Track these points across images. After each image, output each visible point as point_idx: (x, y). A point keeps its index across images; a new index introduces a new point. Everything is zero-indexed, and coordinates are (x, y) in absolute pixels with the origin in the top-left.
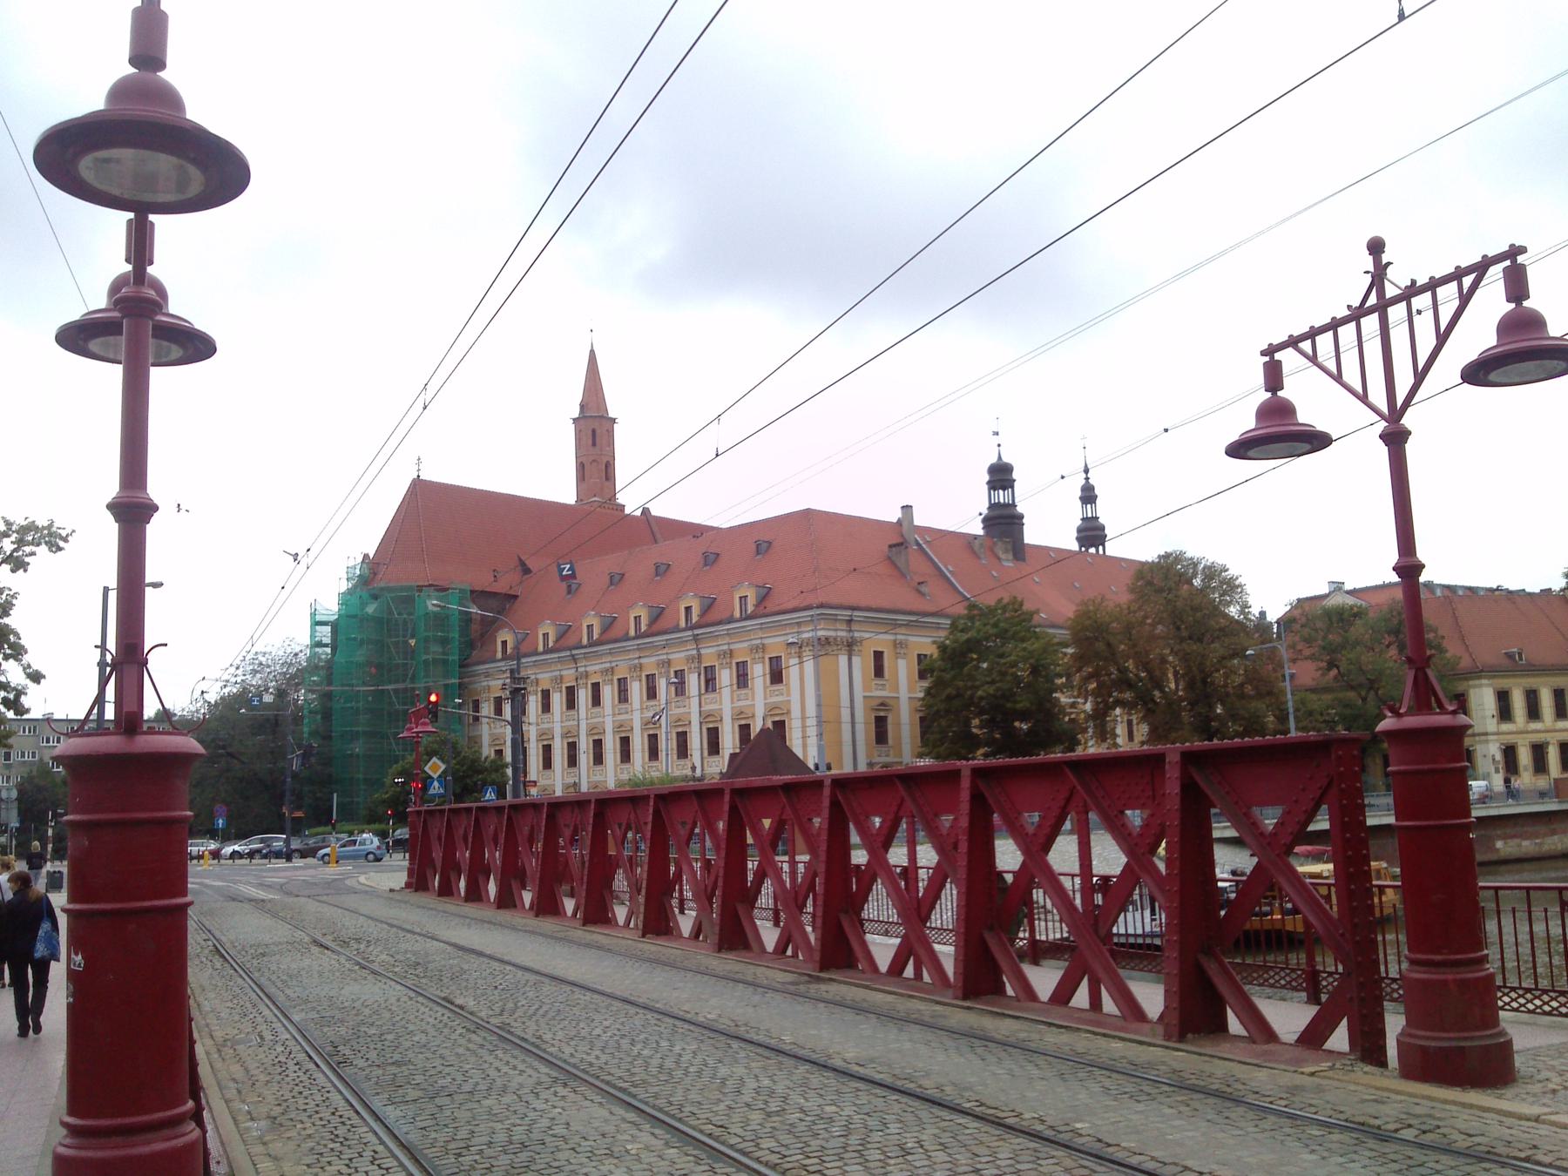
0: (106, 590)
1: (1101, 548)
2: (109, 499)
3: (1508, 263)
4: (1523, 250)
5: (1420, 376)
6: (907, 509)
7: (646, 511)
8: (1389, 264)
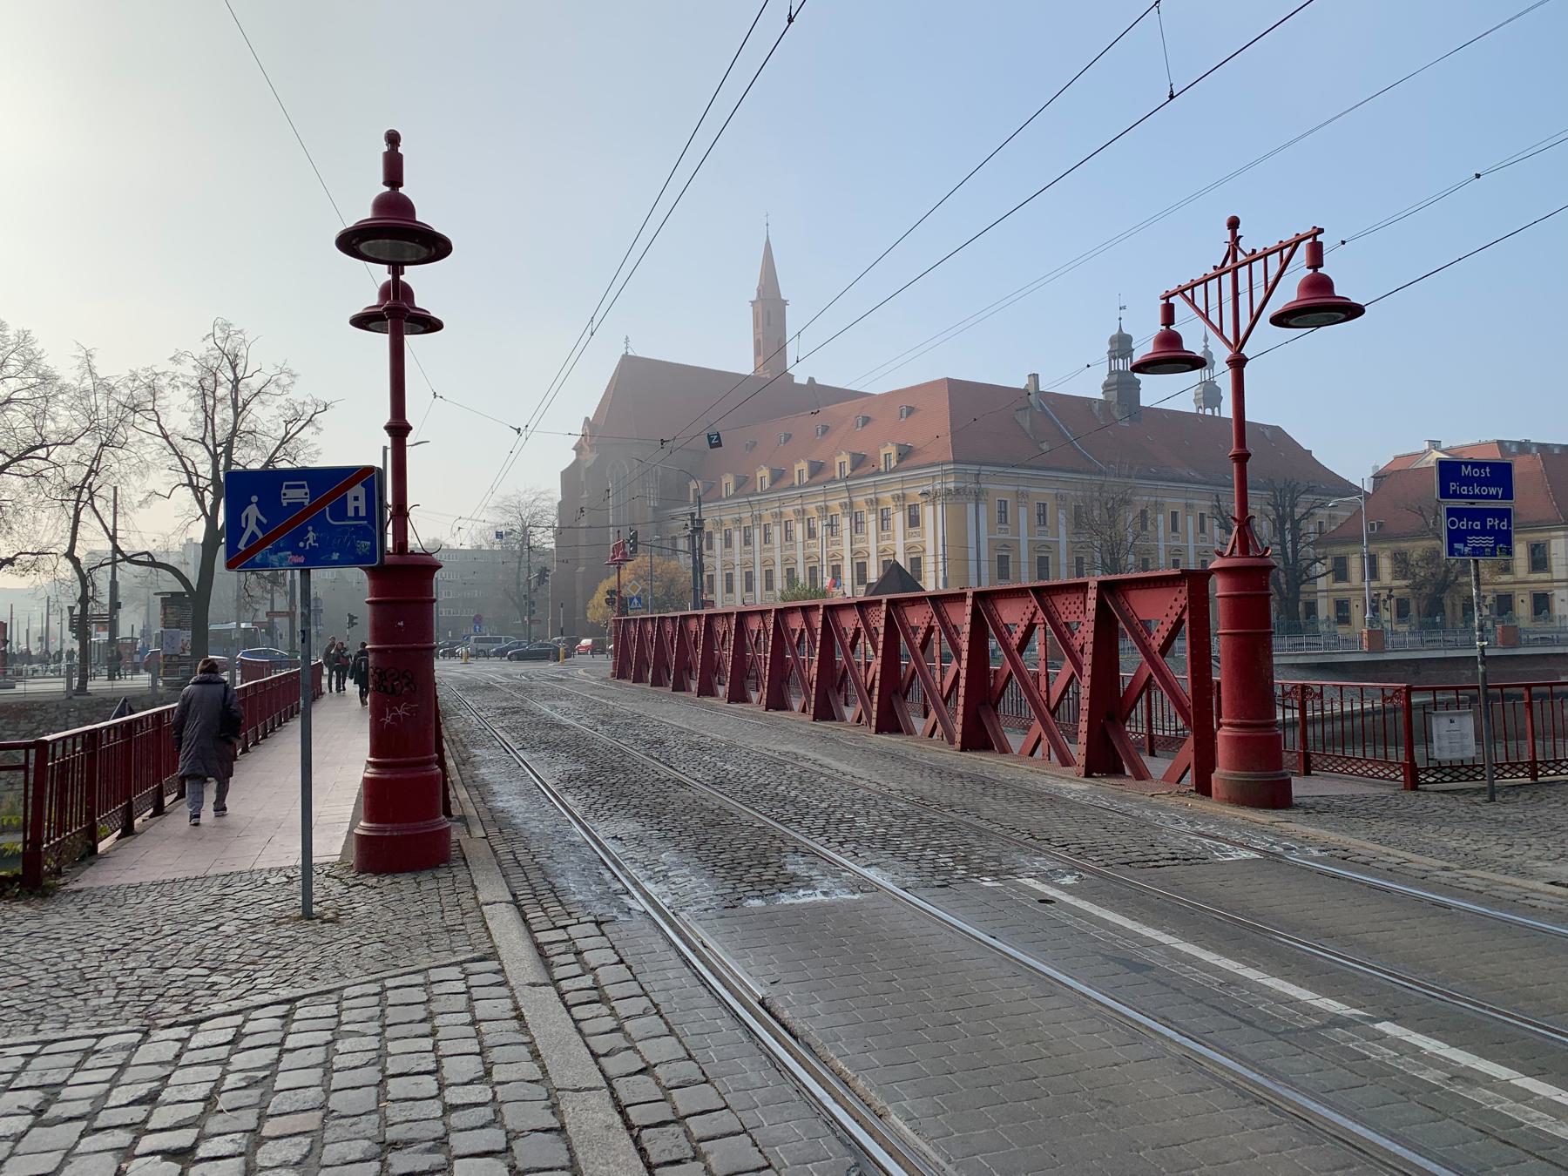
0: (385, 448)
1: (1216, 409)
2: (385, 424)
3: (1310, 240)
4: (1321, 231)
5: (1255, 320)
6: (1035, 377)
7: (811, 380)
8: (1240, 237)
